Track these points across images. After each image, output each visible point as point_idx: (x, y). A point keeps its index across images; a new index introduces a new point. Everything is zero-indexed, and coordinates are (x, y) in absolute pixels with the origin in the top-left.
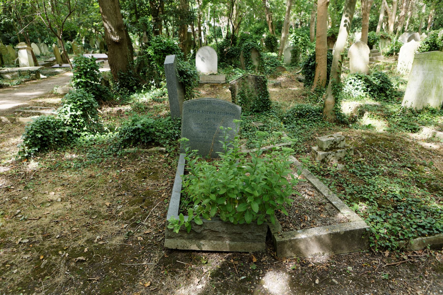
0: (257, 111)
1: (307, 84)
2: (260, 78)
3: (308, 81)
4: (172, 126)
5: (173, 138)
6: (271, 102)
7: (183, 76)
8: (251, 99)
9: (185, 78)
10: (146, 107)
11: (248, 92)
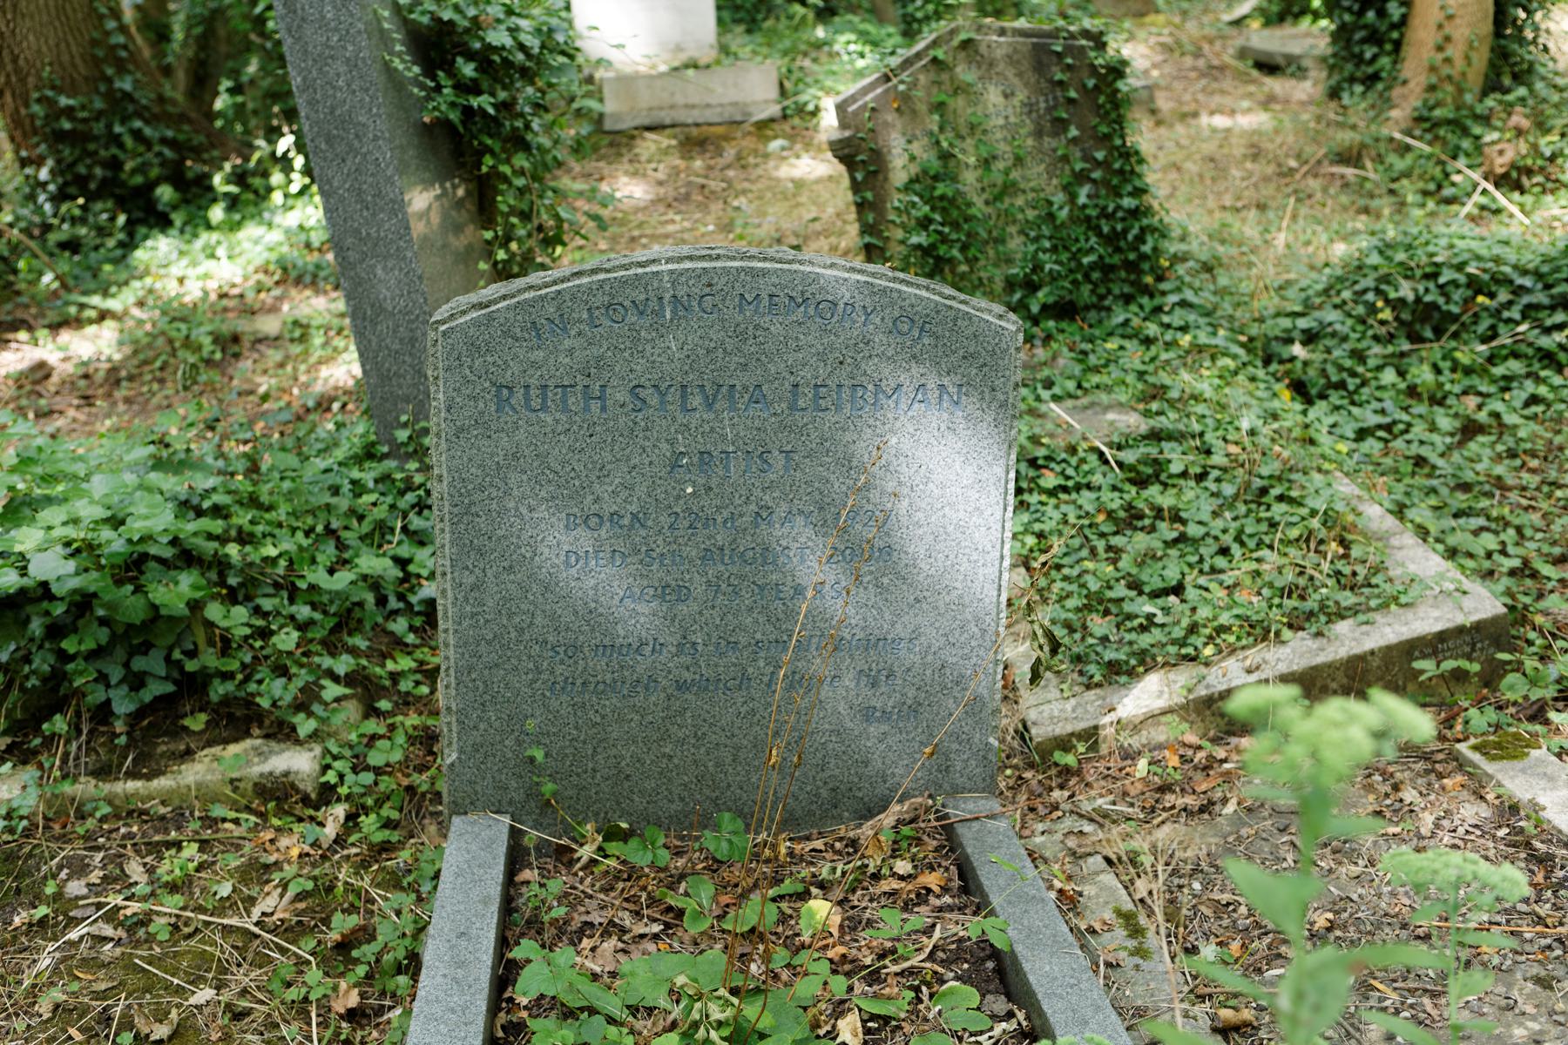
0: (1064, 310)
1: (1352, 80)
2: (1069, 50)
3: (1359, 60)
4: (380, 513)
5: (399, 626)
6: (1162, 232)
7: (452, 72)
8: (1008, 216)
9: (474, 88)
10: (225, 329)
11: (986, 163)
